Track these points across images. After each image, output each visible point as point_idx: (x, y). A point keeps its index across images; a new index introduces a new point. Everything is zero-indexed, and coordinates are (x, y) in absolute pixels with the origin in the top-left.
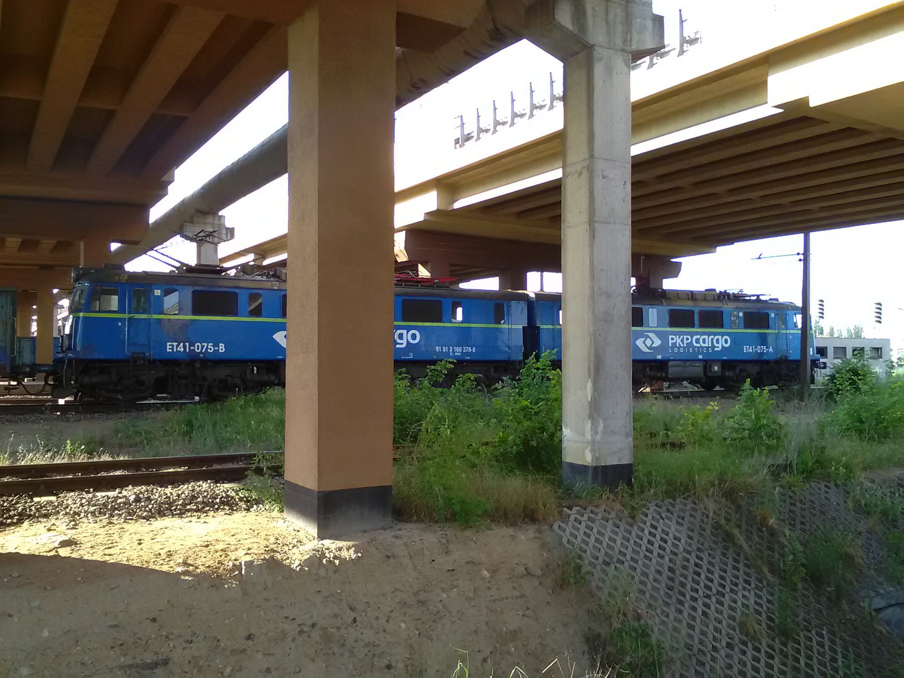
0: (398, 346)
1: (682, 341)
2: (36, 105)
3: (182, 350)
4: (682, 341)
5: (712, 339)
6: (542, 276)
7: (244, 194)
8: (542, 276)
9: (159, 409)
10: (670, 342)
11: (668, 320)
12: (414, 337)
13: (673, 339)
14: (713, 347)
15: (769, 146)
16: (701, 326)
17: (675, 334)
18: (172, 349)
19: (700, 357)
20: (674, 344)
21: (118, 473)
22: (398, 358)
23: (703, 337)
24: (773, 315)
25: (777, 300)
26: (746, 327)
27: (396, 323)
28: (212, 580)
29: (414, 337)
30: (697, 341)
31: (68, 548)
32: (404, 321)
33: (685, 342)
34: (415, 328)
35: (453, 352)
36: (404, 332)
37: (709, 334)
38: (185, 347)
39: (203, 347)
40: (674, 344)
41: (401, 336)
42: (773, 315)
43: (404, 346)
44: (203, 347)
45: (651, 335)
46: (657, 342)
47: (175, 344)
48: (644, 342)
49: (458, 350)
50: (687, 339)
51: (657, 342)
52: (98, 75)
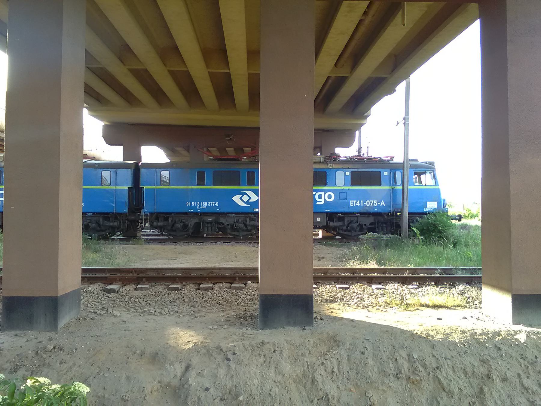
0: (318, 203)
2: (228, 75)
3: (359, 205)
6: (406, 153)
8: (406, 153)
9: (117, 241)
11: (350, 182)
12: (330, 197)
18: (353, 204)
21: (376, 274)
22: (315, 211)
24: (386, 173)
25: (416, 160)
26: (352, 185)
27: (314, 188)
28: (447, 343)
29: (330, 197)
31: (334, 315)
34: (329, 190)
35: (200, 206)
36: (323, 194)
38: (360, 203)
39: (371, 202)
41: (320, 197)
42: (386, 173)
43: (322, 203)
44: (371, 202)
47: (355, 201)
48: (250, 198)
49: (205, 204)
52: (206, 54)
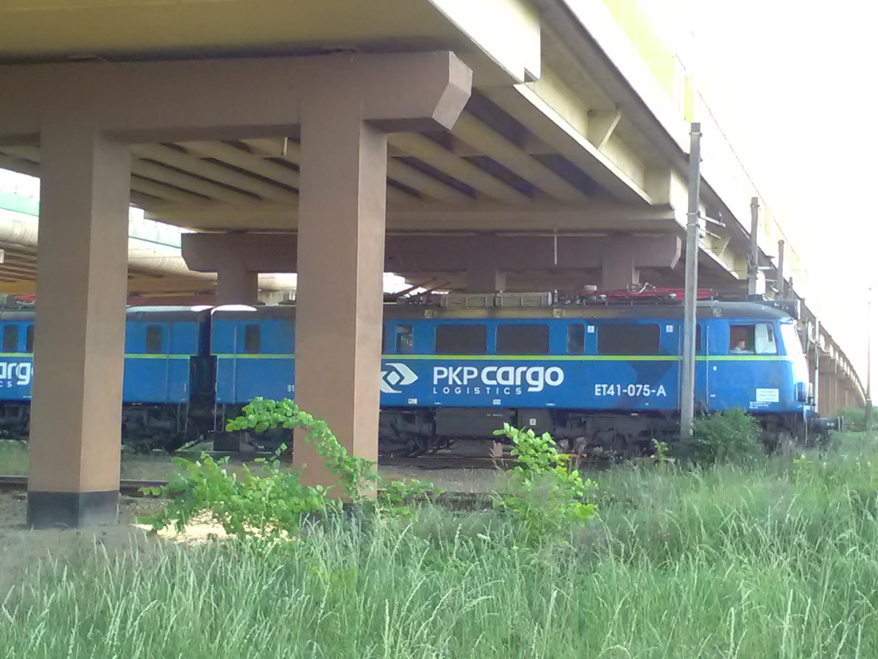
1: (460, 376)
3: (613, 393)
4: (460, 376)
5: (524, 374)
7: (41, 203)
10: (436, 377)
12: (554, 376)
13: (440, 373)
14: (525, 385)
15: (405, 115)
16: (501, 349)
17: (447, 364)
18: (602, 392)
19: (497, 402)
20: (444, 382)
23: (503, 369)
29: (554, 376)
30: (492, 376)
32: (602, 352)
33: (466, 377)
36: (540, 370)
37: (516, 365)
38: (616, 389)
39: (637, 389)
40: (444, 382)
43: (26, 383)
44: (637, 389)
45: (399, 366)
46: (410, 378)
47: (605, 386)
48: (402, 378)
50: (470, 373)
51: (410, 378)
